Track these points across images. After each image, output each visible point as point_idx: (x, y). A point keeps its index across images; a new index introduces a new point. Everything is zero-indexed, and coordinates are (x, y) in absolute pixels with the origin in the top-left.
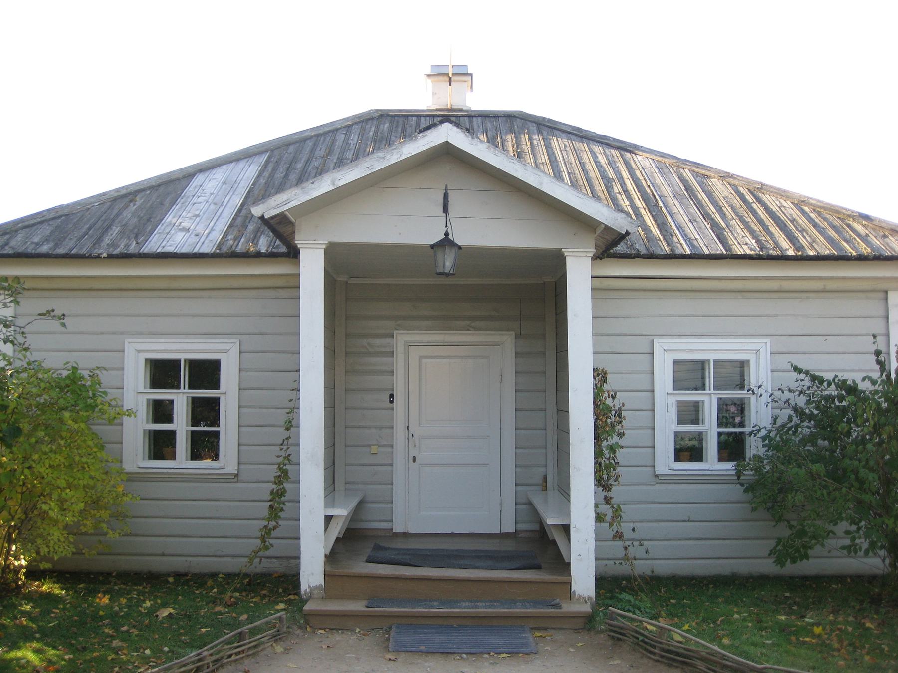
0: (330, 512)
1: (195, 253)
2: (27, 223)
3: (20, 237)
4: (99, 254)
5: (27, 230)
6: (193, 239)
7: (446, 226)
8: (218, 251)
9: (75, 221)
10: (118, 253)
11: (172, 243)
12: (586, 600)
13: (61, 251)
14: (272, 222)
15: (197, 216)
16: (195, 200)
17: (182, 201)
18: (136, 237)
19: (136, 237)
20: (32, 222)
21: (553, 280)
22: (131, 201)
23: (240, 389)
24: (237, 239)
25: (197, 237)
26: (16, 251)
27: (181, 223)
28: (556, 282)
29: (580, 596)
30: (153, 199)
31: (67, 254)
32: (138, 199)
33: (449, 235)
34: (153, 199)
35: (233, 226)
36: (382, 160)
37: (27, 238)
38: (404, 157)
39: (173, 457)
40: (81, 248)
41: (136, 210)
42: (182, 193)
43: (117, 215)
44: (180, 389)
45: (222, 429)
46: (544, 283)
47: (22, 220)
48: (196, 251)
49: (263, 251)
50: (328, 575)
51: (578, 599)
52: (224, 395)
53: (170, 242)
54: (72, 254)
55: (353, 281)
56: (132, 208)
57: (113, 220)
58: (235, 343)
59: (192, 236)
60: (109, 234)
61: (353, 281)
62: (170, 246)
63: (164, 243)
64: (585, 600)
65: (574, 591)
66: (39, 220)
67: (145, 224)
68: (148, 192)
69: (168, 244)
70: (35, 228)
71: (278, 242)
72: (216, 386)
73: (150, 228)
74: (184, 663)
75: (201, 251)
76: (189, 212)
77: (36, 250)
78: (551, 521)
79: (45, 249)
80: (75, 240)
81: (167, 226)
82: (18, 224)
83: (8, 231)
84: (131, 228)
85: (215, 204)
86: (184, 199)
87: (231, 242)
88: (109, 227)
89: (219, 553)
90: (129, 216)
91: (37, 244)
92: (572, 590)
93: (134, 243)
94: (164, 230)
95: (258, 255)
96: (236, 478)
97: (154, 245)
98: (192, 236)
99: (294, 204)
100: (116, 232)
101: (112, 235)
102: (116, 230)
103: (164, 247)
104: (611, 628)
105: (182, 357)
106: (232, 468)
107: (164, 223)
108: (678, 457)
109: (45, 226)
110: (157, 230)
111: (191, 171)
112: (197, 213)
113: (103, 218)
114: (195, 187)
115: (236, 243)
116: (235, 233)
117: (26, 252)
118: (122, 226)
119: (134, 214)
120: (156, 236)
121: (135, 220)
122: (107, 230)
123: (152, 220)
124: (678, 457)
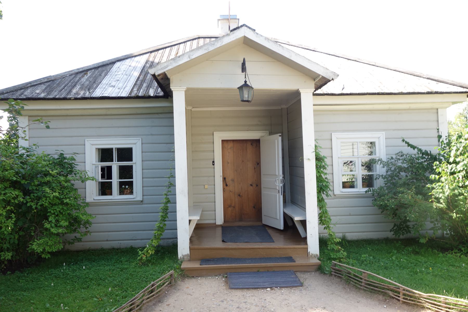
0: (191, 218)
1: (119, 97)
2: (33, 84)
3: (29, 91)
4: (70, 98)
5: (33, 87)
6: (117, 90)
7: (245, 78)
8: (130, 96)
9: (57, 83)
10: (80, 97)
11: (107, 92)
12: (315, 256)
13: (51, 97)
14: (158, 78)
15: (118, 80)
16: (116, 73)
17: (110, 74)
18: (89, 90)
19: (89, 90)
20: (35, 84)
21: (286, 107)
22: (85, 74)
23: (142, 161)
24: (138, 90)
25: (119, 90)
26: (27, 97)
27: (110, 83)
28: (287, 108)
29: (312, 254)
30: (96, 73)
31: (54, 98)
32: (88, 73)
33: (247, 82)
34: (96, 73)
35: (136, 84)
36: (213, 45)
37: (33, 91)
38: (224, 44)
39: (111, 194)
40: (61, 95)
41: (88, 78)
42: (110, 70)
43: (78, 81)
44: (113, 162)
45: (134, 180)
46: (282, 109)
47: (30, 83)
48: (119, 95)
49: (152, 95)
50: (191, 249)
51: (311, 256)
52: (135, 164)
53: (106, 92)
54: (57, 98)
55: (193, 110)
56: (86, 77)
57: (77, 83)
58: (139, 140)
59: (117, 89)
60: (75, 89)
61: (193, 110)
62: (106, 93)
63: (103, 92)
64: (315, 256)
65: (309, 252)
66: (39, 82)
67: (92, 84)
68: (93, 70)
69: (105, 93)
70: (37, 86)
71: (159, 89)
72: (131, 160)
73: (95, 86)
74: (124, 307)
75: (121, 96)
76: (114, 79)
77: (37, 96)
78: (297, 218)
79: (42, 95)
80: (58, 91)
81: (103, 85)
82: (28, 84)
83: (23, 87)
84: (86, 86)
85: (126, 75)
86: (111, 73)
87: (136, 92)
88: (75, 85)
89: (134, 238)
90: (85, 80)
91: (38, 94)
92: (308, 251)
93: (88, 92)
94: (102, 87)
95: (149, 97)
96: (142, 203)
97: (98, 93)
98: (117, 89)
99: (170, 67)
100: (78, 88)
101: (76, 89)
102: (78, 87)
103: (103, 94)
104: (340, 273)
105: (114, 147)
106: (139, 198)
107: (102, 83)
108: (344, 187)
109: (43, 85)
110: (99, 86)
111: (114, 61)
112: (118, 79)
113: (72, 81)
114: (116, 68)
115: (138, 92)
116: (137, 87)
117: (32, 97)
118: (81, 85)
119: (87, 80)
120: (98, 89)
121: (88, 82)
122: (74, 87)
123: (96, 82)
124: (344, 187)
